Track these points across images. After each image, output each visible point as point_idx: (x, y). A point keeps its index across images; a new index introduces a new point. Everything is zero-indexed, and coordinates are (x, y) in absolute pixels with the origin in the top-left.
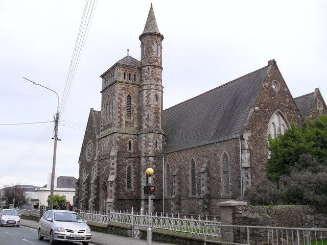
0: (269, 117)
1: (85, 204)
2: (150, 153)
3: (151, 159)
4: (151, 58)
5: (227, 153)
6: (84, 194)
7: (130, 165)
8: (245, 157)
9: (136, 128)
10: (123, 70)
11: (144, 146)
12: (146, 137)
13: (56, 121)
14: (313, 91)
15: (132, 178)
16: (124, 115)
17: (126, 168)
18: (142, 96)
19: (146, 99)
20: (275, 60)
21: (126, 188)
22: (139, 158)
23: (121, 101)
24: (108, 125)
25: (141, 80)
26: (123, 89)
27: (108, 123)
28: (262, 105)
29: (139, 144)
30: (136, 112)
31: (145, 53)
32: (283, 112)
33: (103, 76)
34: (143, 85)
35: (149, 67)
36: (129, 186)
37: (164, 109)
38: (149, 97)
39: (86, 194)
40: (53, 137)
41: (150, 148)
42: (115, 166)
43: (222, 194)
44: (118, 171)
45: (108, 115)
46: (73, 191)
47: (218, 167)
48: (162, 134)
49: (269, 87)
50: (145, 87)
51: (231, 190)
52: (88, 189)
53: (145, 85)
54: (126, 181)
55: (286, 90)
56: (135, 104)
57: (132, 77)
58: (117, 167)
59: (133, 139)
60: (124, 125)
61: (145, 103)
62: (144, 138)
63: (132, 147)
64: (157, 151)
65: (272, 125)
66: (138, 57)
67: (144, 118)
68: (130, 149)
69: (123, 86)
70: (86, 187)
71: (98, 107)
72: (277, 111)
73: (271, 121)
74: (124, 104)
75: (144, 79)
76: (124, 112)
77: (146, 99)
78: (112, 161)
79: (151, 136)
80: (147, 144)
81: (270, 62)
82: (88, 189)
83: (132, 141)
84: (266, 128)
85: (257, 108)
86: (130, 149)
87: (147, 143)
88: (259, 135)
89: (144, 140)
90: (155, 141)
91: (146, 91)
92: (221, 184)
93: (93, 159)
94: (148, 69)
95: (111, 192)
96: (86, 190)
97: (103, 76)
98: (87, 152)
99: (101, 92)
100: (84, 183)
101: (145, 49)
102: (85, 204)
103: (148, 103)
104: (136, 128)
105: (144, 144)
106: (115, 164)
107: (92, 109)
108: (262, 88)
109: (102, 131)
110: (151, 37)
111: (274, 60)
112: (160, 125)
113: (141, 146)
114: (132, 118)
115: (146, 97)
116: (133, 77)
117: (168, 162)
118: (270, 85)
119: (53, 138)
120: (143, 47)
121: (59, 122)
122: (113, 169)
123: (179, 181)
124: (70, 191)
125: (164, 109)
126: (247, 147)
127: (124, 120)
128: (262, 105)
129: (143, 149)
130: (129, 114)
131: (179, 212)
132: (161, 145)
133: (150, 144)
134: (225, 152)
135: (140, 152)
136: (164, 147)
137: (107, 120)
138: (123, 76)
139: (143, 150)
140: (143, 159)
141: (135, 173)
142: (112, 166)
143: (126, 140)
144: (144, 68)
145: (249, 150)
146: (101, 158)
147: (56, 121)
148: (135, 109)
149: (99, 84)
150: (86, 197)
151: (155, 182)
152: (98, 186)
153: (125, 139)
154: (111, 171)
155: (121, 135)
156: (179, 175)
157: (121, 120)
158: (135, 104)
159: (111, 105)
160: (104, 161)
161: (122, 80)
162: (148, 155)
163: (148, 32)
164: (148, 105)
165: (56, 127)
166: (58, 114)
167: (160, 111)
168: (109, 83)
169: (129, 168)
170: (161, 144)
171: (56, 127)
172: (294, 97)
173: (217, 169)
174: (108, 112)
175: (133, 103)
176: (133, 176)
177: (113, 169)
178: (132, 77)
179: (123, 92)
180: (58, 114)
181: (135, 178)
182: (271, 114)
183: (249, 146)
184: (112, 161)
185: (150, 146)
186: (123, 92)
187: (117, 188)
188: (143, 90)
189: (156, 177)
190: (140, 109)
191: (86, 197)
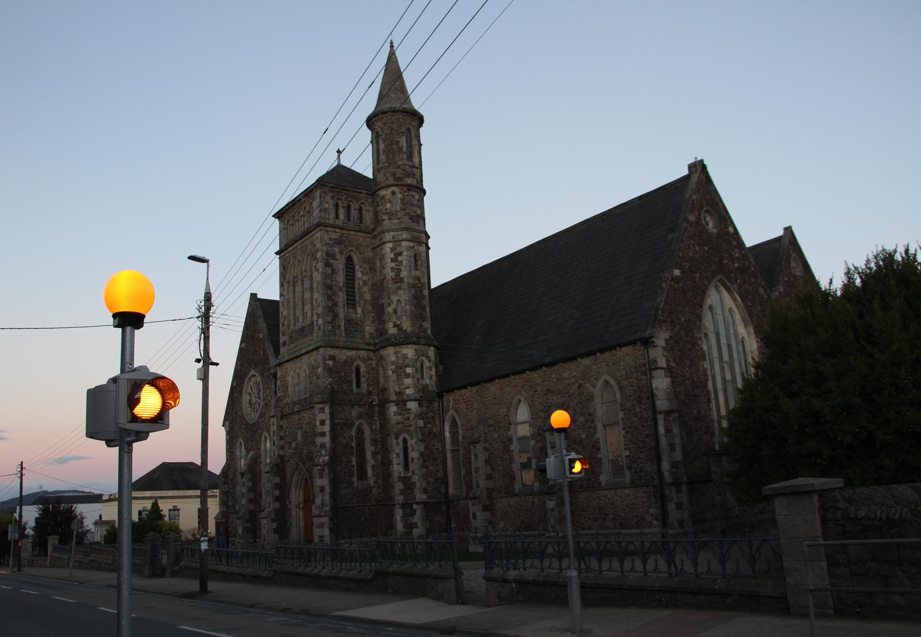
0: (703, 293)
1: (249, 525)
2: (409, 391)
3: (413, 405)
4: (398, 167)
5: (612, 381)
6: (244, 501)
7: (360, 424)
8: (661, 383)
9: (370, 334)
10: (332, 197)
11: (394, 377)
12: (396, 353)
13: (205, 317)
14: (780, 233)
15: (368, 455)
16: (340, 305)
17: (353, 432)
18: (383, 257)
19: (393, 265)
20: (705, 163)
21: (355, 479)
22: (383, 404)
23: (333, 271)
24: (302, 330)
25: (377, 221)
26: (338, 242)
27: (300, 325)
28: (687, 265)
29: (381, 372)
30: (368, 297)
31: (382, 157)
32: (730, 281)
33: (279, 215)
34: (383, 232)
35: (395, 189)
36: (362, 475)
37: (433, 287)
38: (400, 258)
39: (250, 501)
40: (199, 357)
41: (408, 381)
42: (327, 428)
43: (603, 479)
44: (333, 439)
45: (300, 307)
46: (197, 497)
47: (590, 415)
48: (435, 346)
49: (697, 223)
50: (388, 236)
51: (629, 468)
52: (254, 487)
53: (389, 230)
54: (354, 462)
55: (731, 230)
56: (365, 278)
57: (354, 213)
58: (332, 429)
59: (364, 361)
60: (343, 328)
61: (390, 274)
62: (393, 358)
63: (363, 380)
64: (425, 387)
65: (709, 312)
66: (364, 166)
67: (390, 310)
68: (358, 385)
69: (334, 236)
70: (250, 484)
71: (271, 291)
72: (718, 277)
73: (708, 301)
74: (341, 278)
75: (385, 217)
76: (341, 297)
77: (393, 265)
78: (320, 416)
79: (409, 351)
80: (400, 371)
81: (691, 167)
82: (254, 487)
83: (361, 364)
84: (700, 317)
85: (677, 272)
86: (358, 385)
87: (400, 368)
88: (687, 335)
89: (393, 363)
90: (419, 364)
91: (390, 245)
92: (599, 456)
93: (262, 415)
94: (393, 193)
95: (322, 489)
96: (250, 490)
97: (279, 215)
98: (245, 398)
99: (277, 253)
100: (242, 474)
101: (382, 146)
102: (249, 525)
103: (398, 274)
104: (370, 334)
105: (394, 372)
106: (328, 422)
107: (253, 296)
108: (673, 231)
109: (285, 344)
110: (396, 122)
111: (702, 161)
112: (427, 325)
113: (386, 378)
114: (359, 310)
115: (393, 260)
116: (353, 219)
117: (452, 412)
118: (699, 218)
119: (198, 361)
120: (377, 143)
121: (211, 319)
122: (323, 434)
123: (487, 453)
124: (190, 497)
125: (433, 287)
126: (662, 363)
127: (342, 316)
128: (687, 265)
129: (391, 384)
130: (351, 302)
131: (173, 574)
132: (433, 372)
133: (409, 370)
134: (606, 377)
135: (384, 390)
136: (439, 376)
137: (296, 320)
138: (333, 211)
139: (393, 388)
140: (393, 408)
141: (374, 442)
142: (319, 429)
143: (348, 362)
144: (382, 193)
145: (669, 371)
146: (287, 410)
147: (205, 317)
148: (365, 289)
149: (271, 235)
150: (251, 506)
151: (424, 461)
152: (283, 478)
153: (346, 361)
154: (319, 440)
155: (336, 352)
156: (486, 441)
157: (336, 316)
158: (365, 278)
159: (307, 283)
160: (296, 417)
161: (331, 221)
162: (405, 398)
163: (386, 107)
164: (398, 279)
165: (205, 331)
166: (208, 297)
167: (426, 292)
168: (297, 229)
169: (360, 431)
170: (433, 369)
171: (205, 331)
172: (749, 243)
173: (587, 421)
174: (299, 301)
175: (359, 274)
176: (369, 450)
177: (323, 434)
178: (354, 213)
179: (337, 250)
180: (208, 297)
181: (374, 455)
182: (705, 285)
183: (668, 361)
184: (320, 416)
185: (408, 376)
186: (337, 250)
187: (334, 482)
188: (384, 243)
189: (426, 448)
190: (379, 288)
191: (251, 506)
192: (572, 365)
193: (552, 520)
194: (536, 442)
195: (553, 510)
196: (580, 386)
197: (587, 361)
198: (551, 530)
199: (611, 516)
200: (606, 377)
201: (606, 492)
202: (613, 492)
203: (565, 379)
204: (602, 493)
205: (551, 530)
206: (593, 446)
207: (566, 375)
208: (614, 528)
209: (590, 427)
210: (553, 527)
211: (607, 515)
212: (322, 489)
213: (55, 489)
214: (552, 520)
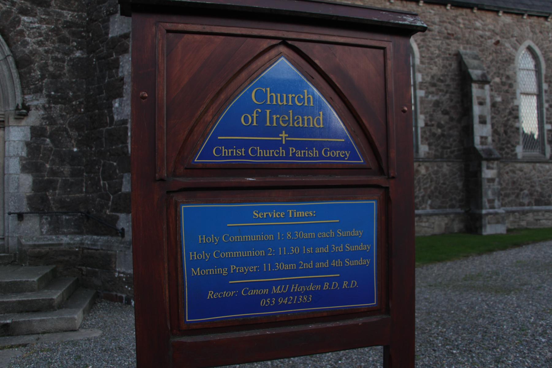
47: (508, 77)
173: (503, 84)
192: (489, 17)
193: (490, 193)
194: (428, 93)
195: (492, 180)
196: (497, 43)
197: (507, 19)
198: (487, 205)
199: (526, 192)
200: (528, 43)
201: (525, 165)
202: (530, 166)
203: (477, 29)
204: (518, 165)
205: (487, 205)
206: (510, 113)
207: (478, 24)
208: (529, 204)
209: (507, 92)
210: (491, 201)
211: (522, 190)
212: (483, 121)
213: (198, 30)
214: (490, 193)
